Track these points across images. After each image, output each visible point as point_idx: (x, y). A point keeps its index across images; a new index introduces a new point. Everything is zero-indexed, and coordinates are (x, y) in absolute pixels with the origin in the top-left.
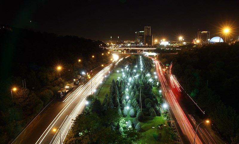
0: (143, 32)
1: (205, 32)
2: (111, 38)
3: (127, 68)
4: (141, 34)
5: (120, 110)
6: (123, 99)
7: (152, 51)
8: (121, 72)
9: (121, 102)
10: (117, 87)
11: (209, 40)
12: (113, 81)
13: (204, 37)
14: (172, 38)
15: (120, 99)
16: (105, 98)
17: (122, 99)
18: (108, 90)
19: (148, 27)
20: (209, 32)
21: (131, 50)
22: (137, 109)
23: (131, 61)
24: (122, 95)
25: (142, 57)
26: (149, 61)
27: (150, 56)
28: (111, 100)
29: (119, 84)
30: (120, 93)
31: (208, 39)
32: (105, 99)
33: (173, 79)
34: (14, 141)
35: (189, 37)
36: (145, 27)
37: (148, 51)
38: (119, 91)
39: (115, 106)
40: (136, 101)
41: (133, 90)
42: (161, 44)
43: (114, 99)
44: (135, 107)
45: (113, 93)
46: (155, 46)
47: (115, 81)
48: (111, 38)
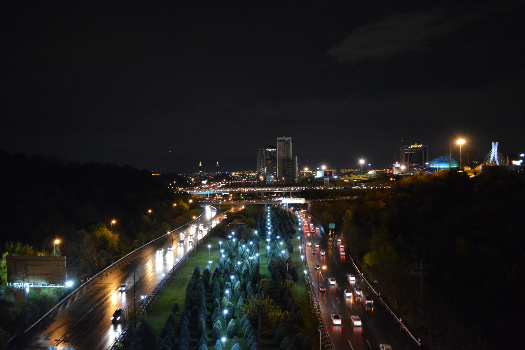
0: (273, 150)
1: (416, 145)
2: (200, 165)
3: (234, 237)
4: (272, 157)
5: (206, 346)
6: (216, 317)
7: (296, 195)
8: (217, 248)
9: (210, 324)
10: (203, 286)
11: (427, 164)
12: (196, 272)
13: (416, 159)
14: (342, 161)
15: (209, 317)
16: (171, 316)
17: (213, 317)
18: (179, 295)
19: (287, 139)
20: (427, 146)
21: (246, 193)
22: (250, 341)
23: (242, 223)
24: (214, 308)
25: (272, 210)
26: (288, 219)
27: (290, 205)
28: (186, 323)
29: (211, 278)
30: (211, 301)
31: (425, 162)
32: (170, 320)
33: (496, 156)
34: (348, 198)
35: (381, 161)
36: (278, 139)
37: (287, 195)
38: (207, 296)
39: (193, 336)
40: (247, 322)
41: (243, 292)
42: (316, 177)
43: (195, 316)
44: (246, 338)
45: (192, 303)
46: (303, 182)
47: (202, 273)
48: (200, 165)
